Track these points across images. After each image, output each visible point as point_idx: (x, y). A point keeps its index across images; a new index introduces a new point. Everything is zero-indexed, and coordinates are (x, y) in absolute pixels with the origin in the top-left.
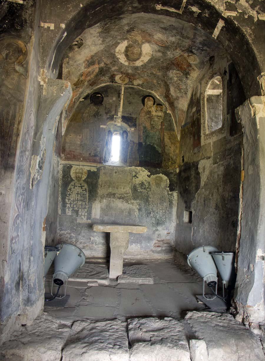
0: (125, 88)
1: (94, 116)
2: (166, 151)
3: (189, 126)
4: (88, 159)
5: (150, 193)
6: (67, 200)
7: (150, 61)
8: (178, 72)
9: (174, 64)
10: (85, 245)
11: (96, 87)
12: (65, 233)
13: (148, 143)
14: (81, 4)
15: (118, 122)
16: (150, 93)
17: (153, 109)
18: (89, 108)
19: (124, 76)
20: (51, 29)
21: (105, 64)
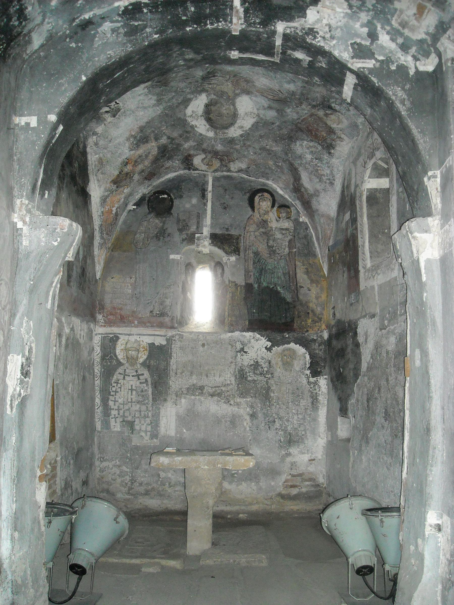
1: (157, 237)
2: (301, 297)
3: (341, 247)
4: (149, 322)
5: (273, 382)
6: (111, 403)
7: (255, 126)
8: (312, 144)
9: (301, 130)
10: (150, 487)
11: (157, 182)
12: (111, 466)
13: (265, 284)
14: (83, 76)
15: (204, 246)
16: (264, 184)
17: (272, 215)
18: (145, 223)
19: (209, 156)
20: (32, 126)
21: (169, 138)
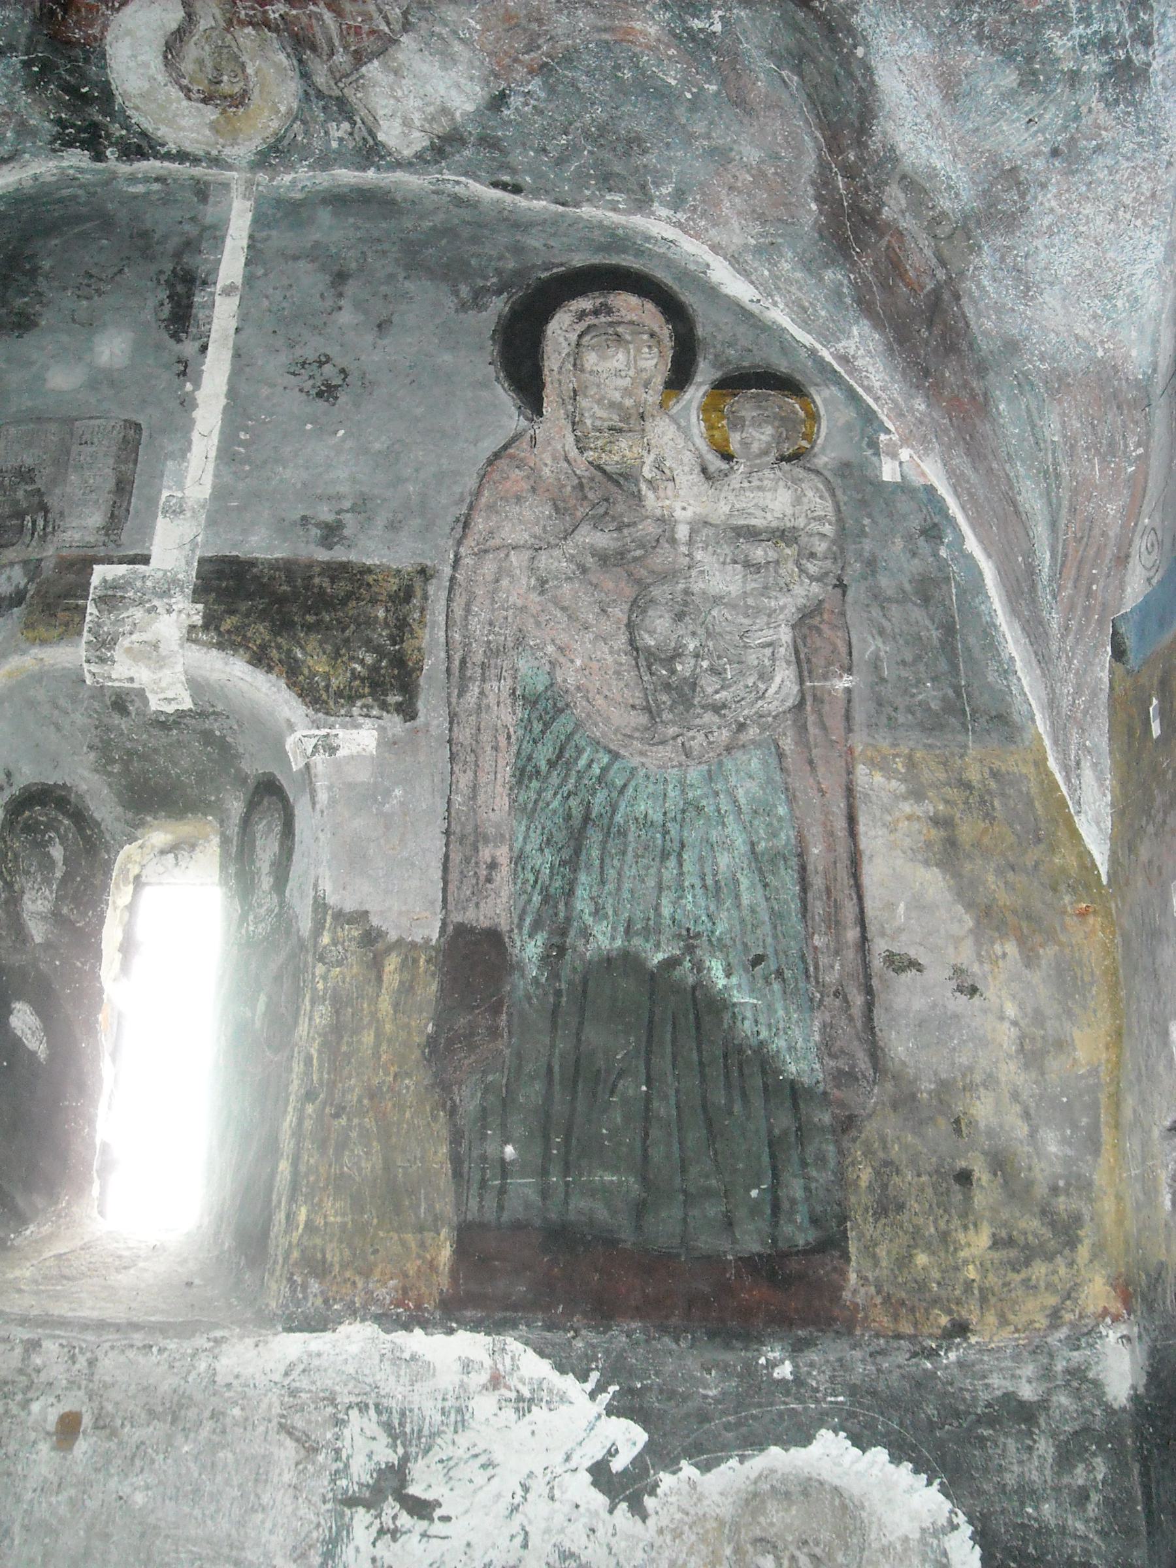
0: (276, 214)
2: (900, 1046)
13: (605, 938)
15: (152, 652)
16: (617, 240)
17: (675, 438)
